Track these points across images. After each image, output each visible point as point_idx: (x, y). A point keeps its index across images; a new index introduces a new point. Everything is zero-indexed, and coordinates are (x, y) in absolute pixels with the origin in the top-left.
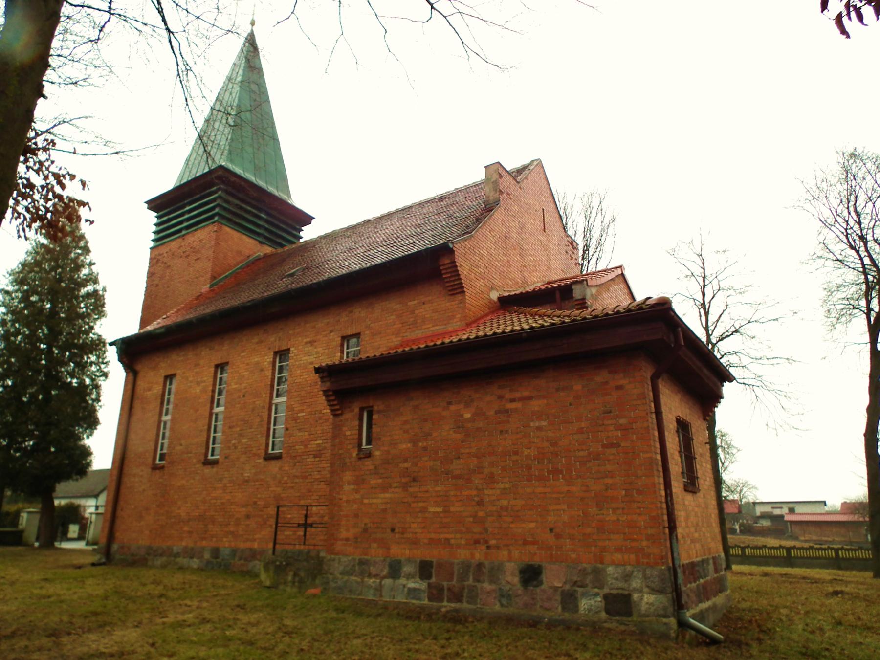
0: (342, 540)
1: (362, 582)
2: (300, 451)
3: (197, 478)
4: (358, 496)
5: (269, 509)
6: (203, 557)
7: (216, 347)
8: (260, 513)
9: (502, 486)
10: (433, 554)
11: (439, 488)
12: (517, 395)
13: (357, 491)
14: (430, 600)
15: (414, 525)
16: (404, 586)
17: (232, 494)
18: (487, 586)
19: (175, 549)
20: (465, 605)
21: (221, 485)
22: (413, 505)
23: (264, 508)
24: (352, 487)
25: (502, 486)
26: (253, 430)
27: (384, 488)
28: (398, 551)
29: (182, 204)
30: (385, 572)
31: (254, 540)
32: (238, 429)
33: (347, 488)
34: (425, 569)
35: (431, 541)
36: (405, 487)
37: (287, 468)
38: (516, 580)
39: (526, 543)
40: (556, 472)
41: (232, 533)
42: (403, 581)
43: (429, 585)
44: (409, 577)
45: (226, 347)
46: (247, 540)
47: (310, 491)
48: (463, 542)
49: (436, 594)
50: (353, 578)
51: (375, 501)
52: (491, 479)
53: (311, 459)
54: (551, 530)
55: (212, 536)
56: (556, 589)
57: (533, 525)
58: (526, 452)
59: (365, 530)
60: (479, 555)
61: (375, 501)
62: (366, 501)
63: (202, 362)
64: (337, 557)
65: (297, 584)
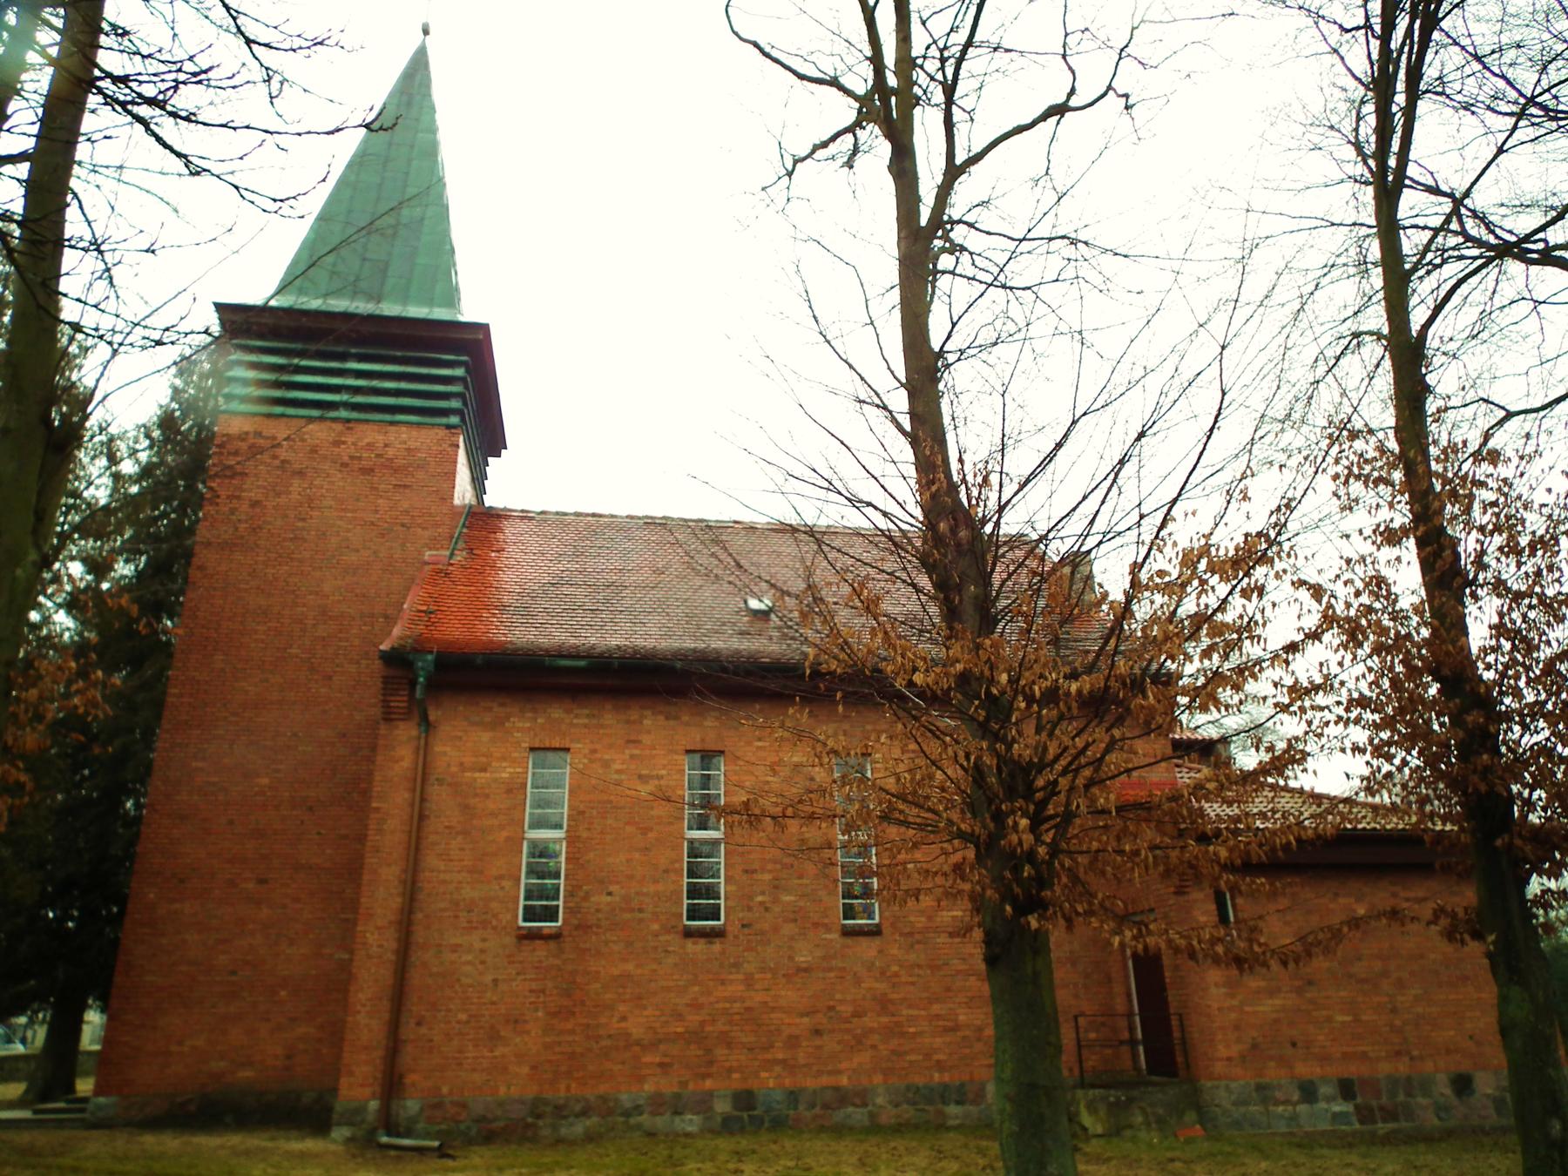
0: (1221, 1059)
1: (1268, 1111)
2: (920, 925)
3: (671, 960)
4: (1235, 1002)
5: (865, 1019)
6: (710, 1108)
7: (685, 718)
8: (847, 1026)
9: (1413, 992)
10: (1353, 1070)
11: (1343, 994)
12: (1412, 895)
13: (1233, 996)
14: (1362, 1122)
15: (1321, 1038)
16: (1327, 1111)
17: (773, 993)
18: (1420, 1100)
19: (625, 1099)
20: (1404, 1124)
21: (740, 977)
22: (1315, 1014)
23: (853, 1016)
24: (1223, 990)
25: (1413, 992)
26: (805, 881)
27: (1272, 992)
28: (1304, 1070)
29: (340, 349)
30: (1296, 1097)
31: (839, 1072)
32: (767, 877)
33: (1213, 990)
34: (1347, 1089)
35: (1345, 1056)
36: (1299, 991)
37: (895, 951)
38: (1448, 1091)
39: (1448, 1052)
40: (1465, 978)
41: (783, 1062)
42: (1322, 1105)
43: (1357, 1107)
44: (1329, 1099)
45: (709, 723)
46: (820, 1073)
47: (948, 989)
48: (1383, 1054)
49: (1365, 1114)
50: (1253, 1108)
51: (1261, 1008)
52: (1401, 985)
53: (942, 939)
54: (1471, 1037)
55: (730, 1070)
56: (1488, 1096)
57: (1452, 1033)
58: (1432, 956)
59: (1255, 1046)
60: (1403, 1067)
61: (1261, 1008)
62: (1247, 1009)
63: (646, 739)
64: (1223, 1083)
65: (1154, 1125)
